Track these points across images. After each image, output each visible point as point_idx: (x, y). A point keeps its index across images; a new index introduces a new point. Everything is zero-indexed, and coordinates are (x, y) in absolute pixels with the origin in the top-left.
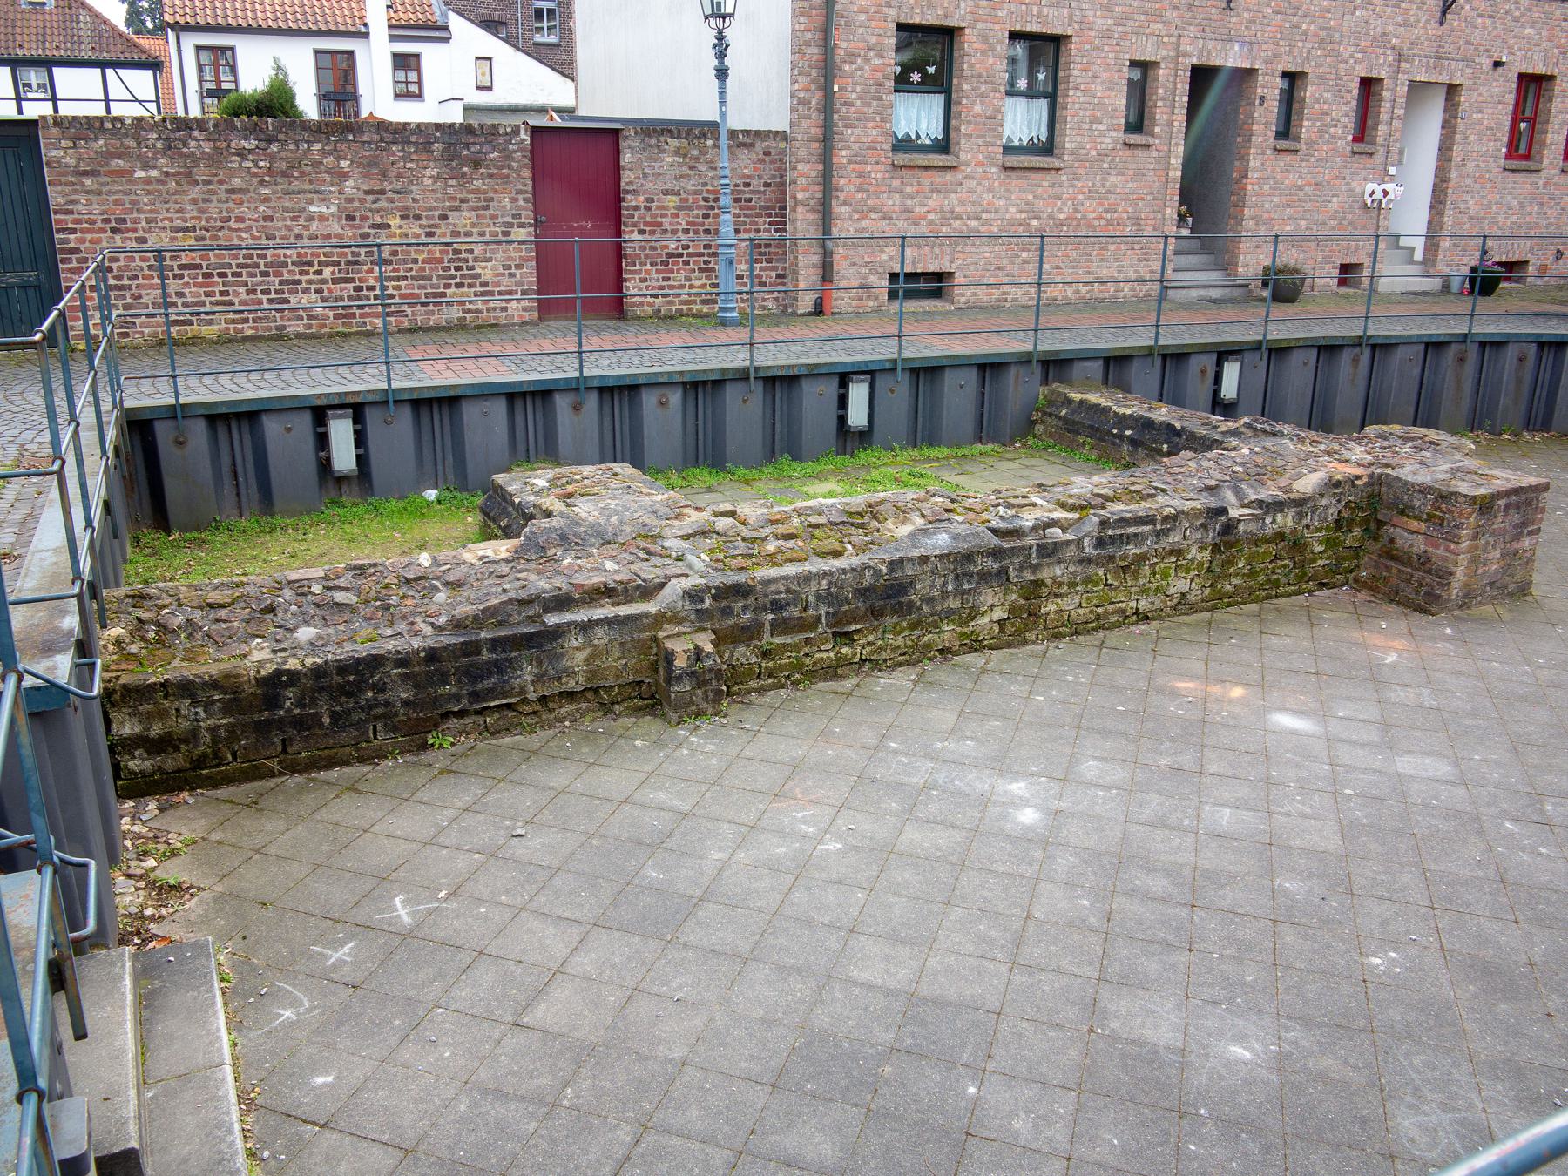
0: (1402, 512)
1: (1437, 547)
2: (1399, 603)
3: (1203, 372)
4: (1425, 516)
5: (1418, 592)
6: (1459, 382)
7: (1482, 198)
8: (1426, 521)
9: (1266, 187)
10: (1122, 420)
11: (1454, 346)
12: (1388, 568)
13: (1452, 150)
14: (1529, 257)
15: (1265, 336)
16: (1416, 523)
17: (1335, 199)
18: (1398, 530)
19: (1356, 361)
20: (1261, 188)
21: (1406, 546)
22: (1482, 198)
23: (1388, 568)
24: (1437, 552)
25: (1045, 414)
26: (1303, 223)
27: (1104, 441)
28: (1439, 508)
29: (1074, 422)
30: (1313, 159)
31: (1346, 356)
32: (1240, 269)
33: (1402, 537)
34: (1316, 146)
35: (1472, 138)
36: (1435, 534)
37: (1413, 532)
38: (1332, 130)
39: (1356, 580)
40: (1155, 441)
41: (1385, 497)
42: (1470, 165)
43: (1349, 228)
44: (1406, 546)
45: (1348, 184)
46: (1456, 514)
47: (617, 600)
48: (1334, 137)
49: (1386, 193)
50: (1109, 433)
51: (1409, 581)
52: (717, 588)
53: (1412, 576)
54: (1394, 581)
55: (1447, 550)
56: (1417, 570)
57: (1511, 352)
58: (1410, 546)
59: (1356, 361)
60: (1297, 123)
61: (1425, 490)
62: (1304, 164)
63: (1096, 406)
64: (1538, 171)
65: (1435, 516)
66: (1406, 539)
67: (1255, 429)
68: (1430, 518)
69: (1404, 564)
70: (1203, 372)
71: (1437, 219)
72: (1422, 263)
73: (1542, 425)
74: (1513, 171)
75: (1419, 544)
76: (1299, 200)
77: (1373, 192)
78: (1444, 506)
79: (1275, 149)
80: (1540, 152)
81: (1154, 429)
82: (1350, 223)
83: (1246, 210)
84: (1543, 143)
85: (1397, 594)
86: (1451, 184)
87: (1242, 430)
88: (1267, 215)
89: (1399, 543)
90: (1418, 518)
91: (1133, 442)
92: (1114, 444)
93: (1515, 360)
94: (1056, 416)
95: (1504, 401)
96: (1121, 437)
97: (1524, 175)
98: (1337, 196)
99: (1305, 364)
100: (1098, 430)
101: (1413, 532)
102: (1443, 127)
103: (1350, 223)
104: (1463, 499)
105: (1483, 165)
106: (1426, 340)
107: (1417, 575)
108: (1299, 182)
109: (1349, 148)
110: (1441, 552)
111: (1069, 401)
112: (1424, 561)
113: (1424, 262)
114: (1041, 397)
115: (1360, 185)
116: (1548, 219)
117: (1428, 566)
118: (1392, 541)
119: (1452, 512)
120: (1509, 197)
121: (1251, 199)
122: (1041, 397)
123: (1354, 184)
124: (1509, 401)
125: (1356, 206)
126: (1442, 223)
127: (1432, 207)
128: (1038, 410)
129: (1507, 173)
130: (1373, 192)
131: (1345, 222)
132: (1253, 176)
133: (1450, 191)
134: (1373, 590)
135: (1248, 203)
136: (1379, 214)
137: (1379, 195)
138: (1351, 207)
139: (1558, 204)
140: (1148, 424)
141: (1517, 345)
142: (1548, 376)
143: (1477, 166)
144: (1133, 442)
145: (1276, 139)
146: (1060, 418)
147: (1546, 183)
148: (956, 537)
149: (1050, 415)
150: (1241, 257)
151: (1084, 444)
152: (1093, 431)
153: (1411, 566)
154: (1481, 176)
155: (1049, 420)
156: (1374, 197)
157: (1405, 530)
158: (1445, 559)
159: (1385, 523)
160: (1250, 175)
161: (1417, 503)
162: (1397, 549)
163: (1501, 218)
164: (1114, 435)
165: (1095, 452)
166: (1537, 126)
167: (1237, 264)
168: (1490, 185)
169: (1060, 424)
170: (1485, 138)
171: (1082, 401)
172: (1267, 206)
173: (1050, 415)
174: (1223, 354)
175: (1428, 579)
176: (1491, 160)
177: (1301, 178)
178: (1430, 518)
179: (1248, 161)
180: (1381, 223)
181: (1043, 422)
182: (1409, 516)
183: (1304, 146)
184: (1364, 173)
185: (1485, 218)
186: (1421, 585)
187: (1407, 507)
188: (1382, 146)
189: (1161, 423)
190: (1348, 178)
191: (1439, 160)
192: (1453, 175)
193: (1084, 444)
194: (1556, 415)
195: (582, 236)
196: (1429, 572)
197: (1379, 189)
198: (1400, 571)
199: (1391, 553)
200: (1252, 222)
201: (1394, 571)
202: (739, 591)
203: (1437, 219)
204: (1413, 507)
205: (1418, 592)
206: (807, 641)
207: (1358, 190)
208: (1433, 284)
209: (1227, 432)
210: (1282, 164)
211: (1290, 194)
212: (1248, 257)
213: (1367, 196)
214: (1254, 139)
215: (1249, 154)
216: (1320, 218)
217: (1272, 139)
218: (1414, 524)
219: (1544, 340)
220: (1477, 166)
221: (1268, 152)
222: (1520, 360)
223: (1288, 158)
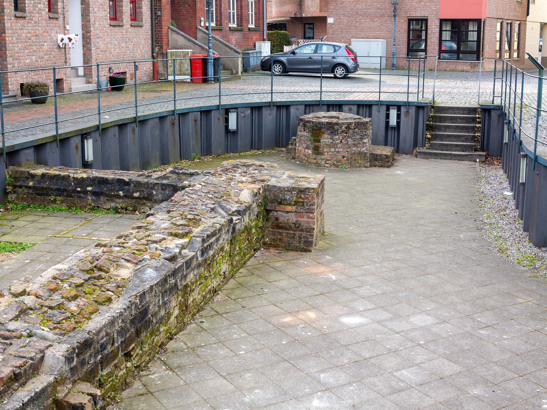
0: (280, 203)
1: (303, 217)
2: (292, 250)
3: (77, 147)
4: (293, 203)
5: (300, 242)
6: (174, 135)
7: (104, 40)
8: (294, 205)
9: (14, 38)
10: (81, 182)
11: (169, 118)
12: (281, 234)
13: (89, 16)
14: (126, 70)
15: (100, 122)
16: (290, 207)
17: (45, 44)
18: (279, 213)
19: (133, 130)
20: (12, 39)
21: (285, 220)
22: (104, 40)
23: (281, 234)
24: (304, 220)
25: (15, 186)
26: (34, 58)
27: (72, 196)
28: (301, 197)
29: (42, 188)
30: (33, 22)
31: (129, 128)
32: (10, 87)
33: (282, 216)
34: (33, 15)
35: (96, 9)
36: (301, 211)
37: (288, 212)
38: (39, 6)
39: (265, 244)
40: (111, 190)
41: (269, 197)
42: (97, 23)
43: (54, 59)
44: (285, 220)
45: (50, 35)
46: (310, 199)
47: (21, 381)
48: (40, 9)
49: (70, 40)
50: (75, 191)
51: (293, 237)
52: (78, 347)
53: (295, 235)
54: (286, 239)
55: (308, 217)
56: (296, 231)
57: (191, 117)
58: (288, 220)
59: (133, 130)
60: (21, 2)
61: (290, 190)
62: (29, 25)
63: (57, 177)
64: (122, 26)
65: (299, 202)
66: (285, 217)
67: (178, 173)
68: (296, 203)
69: (287, 229)
70: (77, 147)
71: (88, 52)
72: (84, 76)
73: (207, 152)
74: (114, 26)
75: (293, 218)
76: (30, 45)
77: (62, 40)
78: (303, 196)
79: (16, 17)
80: (121, 17)
81: (108, 183)
82: (54, 57)
83: (7, 52)
84: (122, 12)
85: (289, 246)
86: (92, 34)
87: (169, 175)
88: (17, 54)
89: (281, 219)
90: (288, 204)
91: (94, 193)
92: (80, 197)
93: (193, 121)
94: (26, 187)
95: (192, 143)
96: (85, 192)
97: (117, 28)
98: (46, 42)
99: (115, 135)
100: (65, 190)
101: (288, 212)
102: (82, 4)
103: (54, 57)
104: (312, 191)
105: (102, 23)
106: (159, 115)
107: (298, 233)
108: (29, 35)
109: (47, 16)
110: (305, 219)
111: (33, 176)
112: (297, 226)
113: (85, 76)
114: (8, 176)
115: (55, 36)
116: (129, 50)
117: (301, 228)
118: (277, 219)
119: (308, 198)
120: (114, 39)
121: (9, 46)
122: (8, 176)
123: (53, 35)
124: (194, 143)
125: (55, 47)
126: (91, 54)
127: (84, 46)
128: (9, 184)
129: (112, 27)
130: (62, 40)
131: (52, 56)
132: (8, 32)
133: (92, 37)
134: (276, 247)
135: (8, 48)
136: (65, 51)
137: (66, 41)
138: (53, 48)
139: (132, 42)
140: (103, 181)
141: (193, 114)
142: (205, 128)
143: (100, 24)
144: (94, 193)
145: (15, 11)
146: (30, 187)
147: (126, 32)
148: (156, 269)
149: (20, 187)
150: (9, 80)
151: (55, 200)
152: (60, 192)
153: (291, 230)
154: (102, 29)
155: (20, 190)
156: (64, 42)
157: (283, 212)
158: (308, 223)
159: (271, 211)
160: (7, 31)
161: (288, 197)
162: (281, 223)
163: (113, 50)
164: (79, 192)
165: (65, 205)
166: (117, 3)
167: (7, 84)
168: (106, 34)
169: (31, 191)
170: (101, 10)
171: (43, 175)
172: (16, 49)
173: (20, 187)
174: (84, 135)
175: (304, 234)
176: (104, 21)
177: (29, 33)
178: (296, 203)
179: (4, 24)
180: (67, 56)
181: (15, 192)
182: (284, 204)
183: (28, 15)
184: (56, 29)
185: (107, 51)
186: (300, 238)
187: (282, 200)
188: (61, 14)
189: (113, 179)
190: (49, 32)
191: (83, 21)
192: (92, 29)
193: (55, 200)
194: (213, 147)
195: (340, 72)
196: (302, 230)
197: (66, 38)
198: (287, 233)
199: (278, 226)
200: (11, 59)
201: (284, 234)
202: (86, 345)
203: (88, 52)
204: (286, 200)
205: (300, 242)
206: (116, 366)
207: (55, 38)
208: (93, 87)
209: (159, 178)
210: (20, 25)
211: (26, 42)
212: (13, 79)
213: (59, 42)
214: (5, 11)
215: (4, 20)
216: (41, 54)
217: (13, 11)
218: (289, 208)
219: (203, 110)
220: (100, 24)
221: (13, 18)
222: (195, 121)
223: (21, 21)
